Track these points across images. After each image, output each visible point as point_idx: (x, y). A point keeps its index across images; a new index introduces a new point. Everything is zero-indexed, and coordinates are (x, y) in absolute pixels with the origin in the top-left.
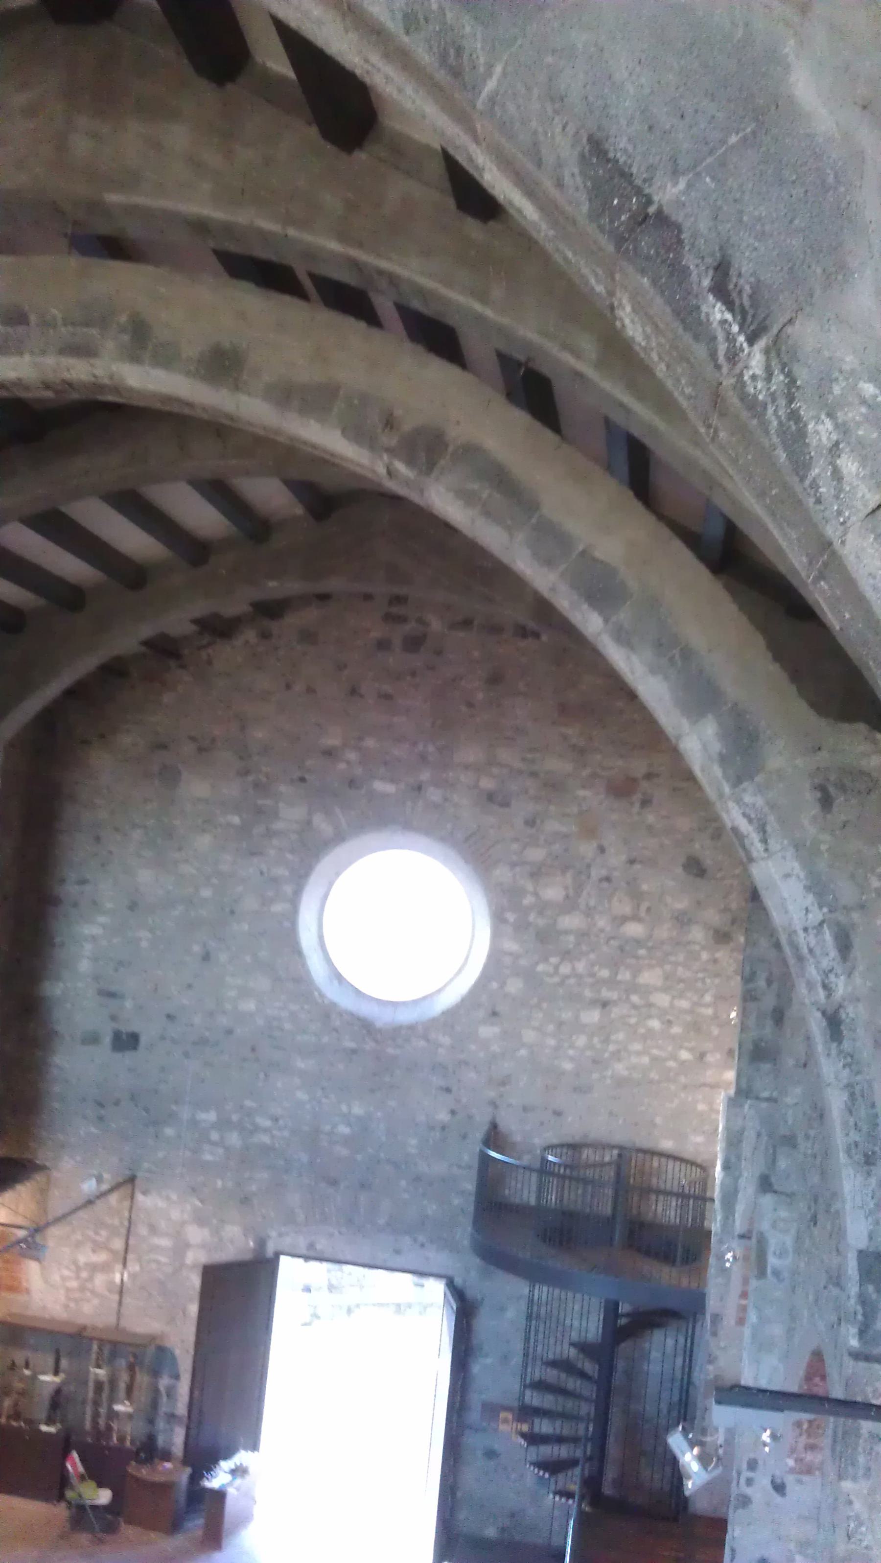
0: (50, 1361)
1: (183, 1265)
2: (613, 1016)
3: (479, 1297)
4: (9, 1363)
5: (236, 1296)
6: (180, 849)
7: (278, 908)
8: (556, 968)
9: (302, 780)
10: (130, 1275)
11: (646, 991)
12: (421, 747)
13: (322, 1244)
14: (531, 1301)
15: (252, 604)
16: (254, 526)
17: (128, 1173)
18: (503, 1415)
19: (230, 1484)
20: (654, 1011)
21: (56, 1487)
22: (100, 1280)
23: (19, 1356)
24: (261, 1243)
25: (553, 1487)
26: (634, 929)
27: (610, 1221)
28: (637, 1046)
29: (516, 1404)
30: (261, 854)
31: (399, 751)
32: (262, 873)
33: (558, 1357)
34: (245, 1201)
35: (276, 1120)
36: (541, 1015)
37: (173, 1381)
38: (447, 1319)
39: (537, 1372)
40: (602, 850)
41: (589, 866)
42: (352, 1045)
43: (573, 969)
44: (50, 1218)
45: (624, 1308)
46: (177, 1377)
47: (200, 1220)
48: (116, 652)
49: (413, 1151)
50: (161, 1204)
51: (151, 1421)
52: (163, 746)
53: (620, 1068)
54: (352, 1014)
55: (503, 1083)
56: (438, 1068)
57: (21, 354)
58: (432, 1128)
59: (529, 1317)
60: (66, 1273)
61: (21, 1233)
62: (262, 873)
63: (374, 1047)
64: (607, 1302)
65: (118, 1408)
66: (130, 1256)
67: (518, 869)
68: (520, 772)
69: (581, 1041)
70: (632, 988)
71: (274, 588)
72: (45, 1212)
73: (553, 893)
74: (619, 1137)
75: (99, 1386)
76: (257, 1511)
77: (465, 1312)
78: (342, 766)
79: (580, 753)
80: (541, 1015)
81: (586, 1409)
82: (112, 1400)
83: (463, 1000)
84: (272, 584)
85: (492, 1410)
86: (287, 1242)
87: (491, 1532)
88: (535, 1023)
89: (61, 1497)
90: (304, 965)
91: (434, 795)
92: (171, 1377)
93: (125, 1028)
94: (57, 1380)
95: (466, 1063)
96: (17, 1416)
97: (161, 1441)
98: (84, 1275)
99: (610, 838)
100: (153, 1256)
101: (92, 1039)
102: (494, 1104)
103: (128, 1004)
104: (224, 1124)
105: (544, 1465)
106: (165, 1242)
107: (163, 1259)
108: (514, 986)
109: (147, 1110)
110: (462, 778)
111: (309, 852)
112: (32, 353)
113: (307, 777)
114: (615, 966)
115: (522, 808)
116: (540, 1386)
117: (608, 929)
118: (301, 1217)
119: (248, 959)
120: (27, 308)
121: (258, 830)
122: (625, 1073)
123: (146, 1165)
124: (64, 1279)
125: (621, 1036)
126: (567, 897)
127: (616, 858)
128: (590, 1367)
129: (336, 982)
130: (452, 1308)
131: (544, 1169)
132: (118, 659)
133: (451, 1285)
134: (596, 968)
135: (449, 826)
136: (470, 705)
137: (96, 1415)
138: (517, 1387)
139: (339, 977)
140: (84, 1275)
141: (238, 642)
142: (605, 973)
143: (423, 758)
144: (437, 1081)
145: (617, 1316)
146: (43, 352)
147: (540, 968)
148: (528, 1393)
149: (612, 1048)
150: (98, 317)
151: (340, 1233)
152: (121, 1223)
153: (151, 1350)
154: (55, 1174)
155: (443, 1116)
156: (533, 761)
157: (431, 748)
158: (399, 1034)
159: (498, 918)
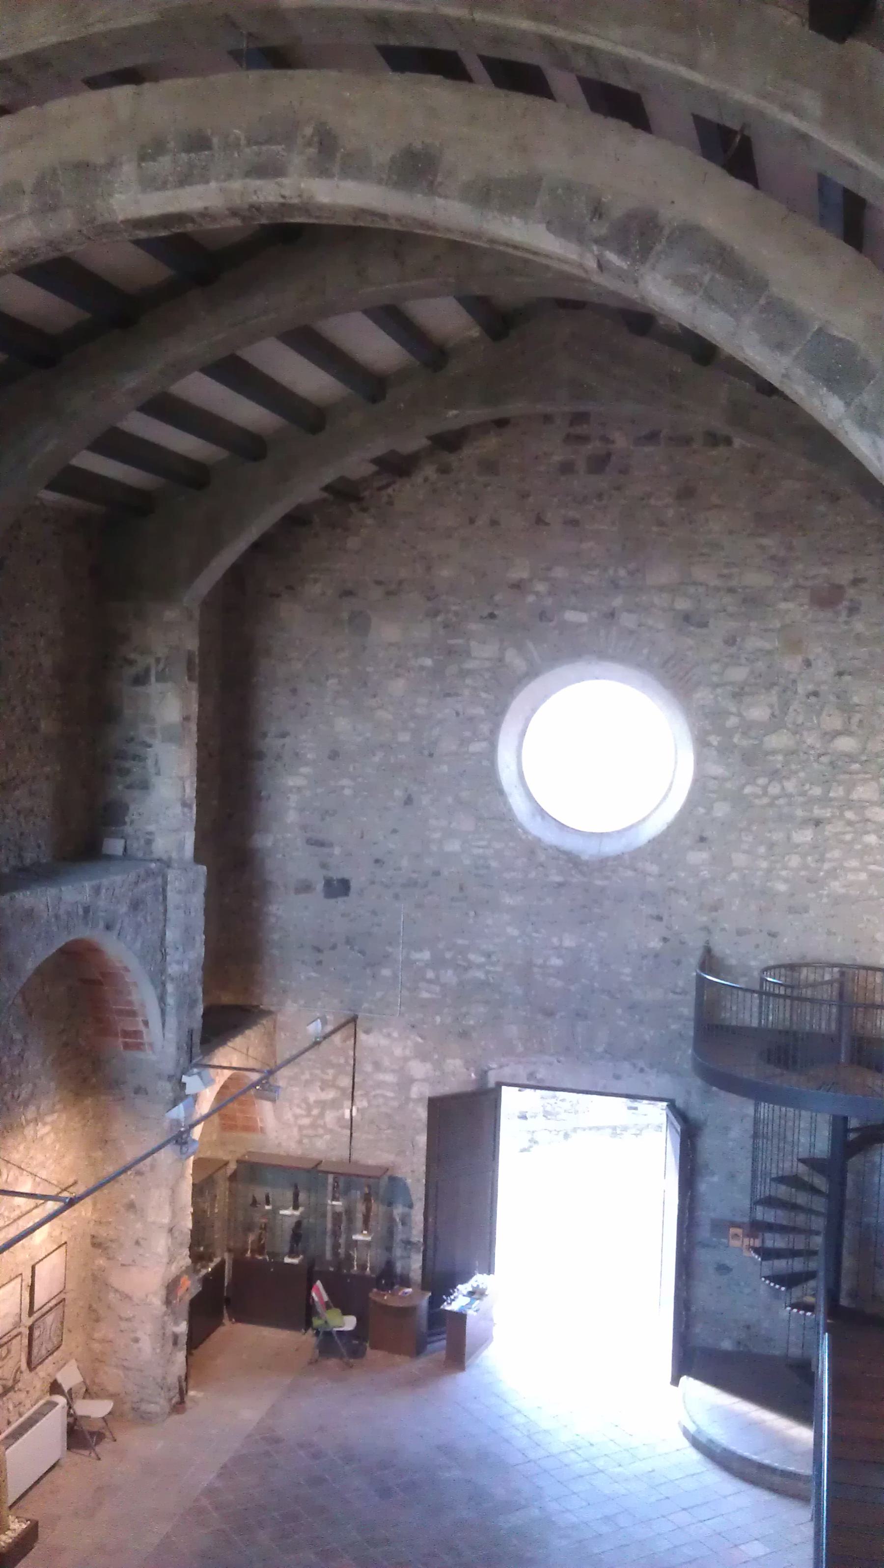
0: (289, 1195)
1: (408, 1099)
2: (826, 833)
3: (702, 1118)
4: (250, 1201)
5: (462, 1127)
6: (375, 696)
7: (476, 747)
8: (765, 788)
9: (492, 616)
10: (358, 1110)
11: (861, 806)
12: (611, 572)
13: (542, 1073)
14: (756, 1121)
15: (430, 438)
16: (430, 352)
17: (351, 1014)
18: (733, 1230)
19: (469, 1305)
20: (870, 826)
21: (303, 1316)
22: (330, 1117)
23: (260, 1193)
24: (483, 1075)
25: (788, 1302)
26: (846, 744)
27: (833, 1040)
28: (854, 863)
29: (746, 1220)
30: (457, 695)
31: (589, 578)
32: (458, 714)
33: (787, 1173)
34: (464, 1035)
35: (488, 955)
36: (750, 839)
37: (407, 1209)
38: (672, 1139)
39: (766, 1189)
40: (808, 663)
41: (794, 682)
42: (559, 879)
43: (783, 788)
44: (279, 1062)
45: (853, 1123)
46: (411, 1206)
47: (423, 1056)
48: (301, 500)
49: (629, 979)
50: (384, 1042)
51: (389, 1249)
52: (348, 593)
53: (836, 886)
54: (557, 849)
55: (715, 908)
56: (647, 896)
57: (207, 182)
58: (644, 957)
59: (755, 1136)
60: (298, 1111)
61: (255, 1077)
62: (458, 714)
63: (581, 879)
64: (835, 1117)
65: (357, 1237)
66: (357, 1093)
67: (719, 691)
68: (717, 589)
69: (794, 861)
70: (848, 803)
71: (454, 418)
72: (274, 1054)
73: (758, 713)
74: (839, 955)
75: (337, 1216)
76: (496, 1332)
77: (689, 1134)
78: (531, 599)
79: (780, 564)
80: (750, 839)
81: (819, 1223)
82: (351, 1231)
83: (670, 827)
84: (452, 413)
85: (721, 1227)
86: (507, 1073)
87: (727, 1345)
88: (745, 847)
89: (308, 1324)
90: (506, 803)
91: (628, 620)
92: (404, 1205)
93: (336, 875)
94: (297, 1213)
95: (676, 891)
96: (260, 1249)
97: (399, 1267)
98: (315, 1112)
99: (816, 650)
100: (378, 1092)
101: (305, 887)
102: (706, 929)
103: (337, 851)
104: (438, 962)
105: (777, 1279)
106: (389, 1078)
107: (390, 1094)
108: (721, 810)
109: (362, 952)
110: (656, 600)
111: (502, 689)
112: (217, 180)
113: (496, 612)
114: (827, 784)
115: (721, 627)
116: (770, 1202)
117: (818, 746)
118: (520, 1048)
119: (450, 800)
120: (209, 132)
121: (452, 669)
122: (842, 891)
123: (366, 1005)
124: (296, 1117)
125: (836, 854)
126: (773, 715)
127: (823, 672)
128: (820, 1182)
129: (539, 819)
130: (677, 1130)
131: (764, 994)
132: (299, 507)
133: (672, 1106)
134: (807, 787)
135: (645, 651)
136: (661, 524)
137: (336, 1246)
138: (746, 1203)
139: (542, 813)
140: (315, 1112)
141: (418, 478)
142: (817, 791)
143: (615, 585)
144: (647, 909)
145: (847, 1131)
146: (229, 176)
147: (748, 790)
148: (759, 1208)
149: (827, 866)
150: (282, 131)
151: (559, 1061)
152: (346, 1062)
153: (384, 1181)
154: (280, 1018)
155: (655, 944)
156: (729, 577)
157: (622, 572)
158: (604, 865)
159: (701, 742)
